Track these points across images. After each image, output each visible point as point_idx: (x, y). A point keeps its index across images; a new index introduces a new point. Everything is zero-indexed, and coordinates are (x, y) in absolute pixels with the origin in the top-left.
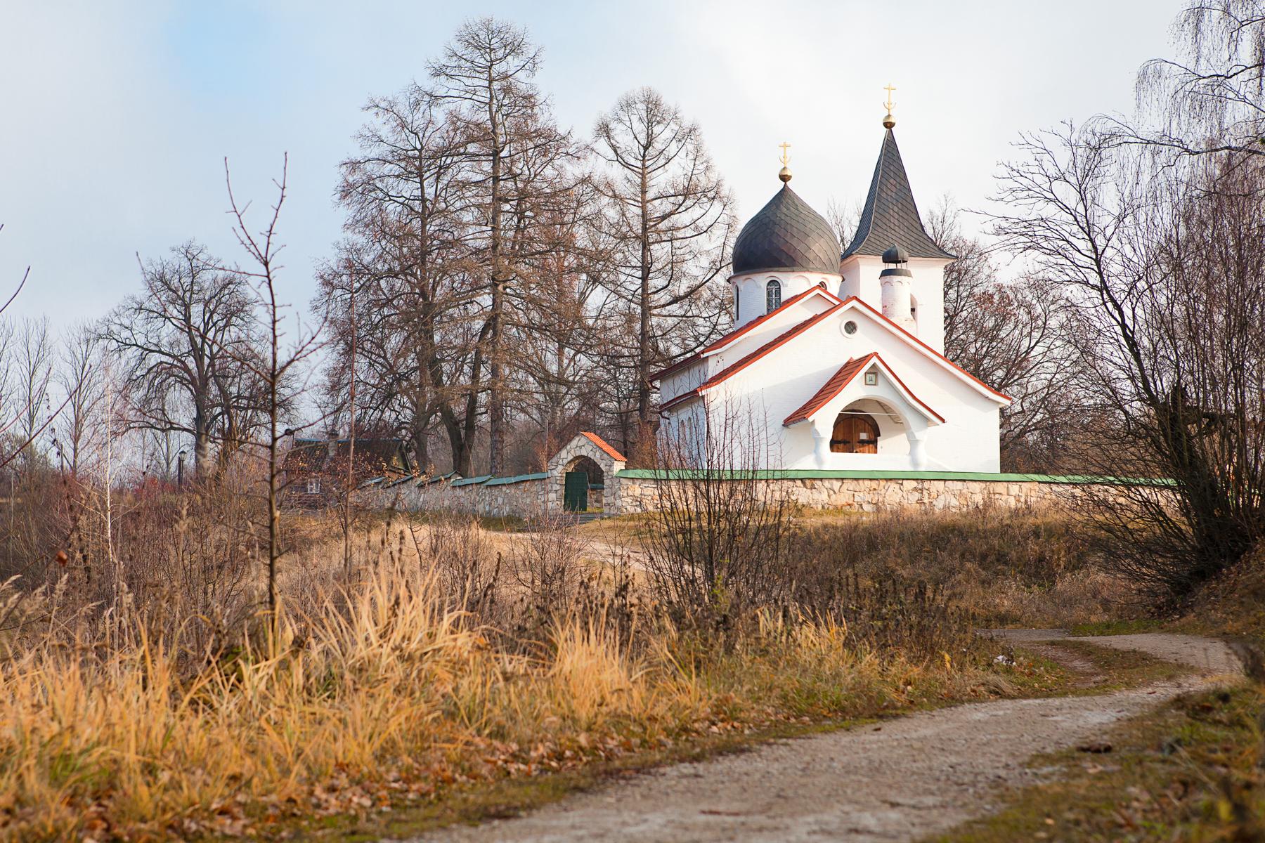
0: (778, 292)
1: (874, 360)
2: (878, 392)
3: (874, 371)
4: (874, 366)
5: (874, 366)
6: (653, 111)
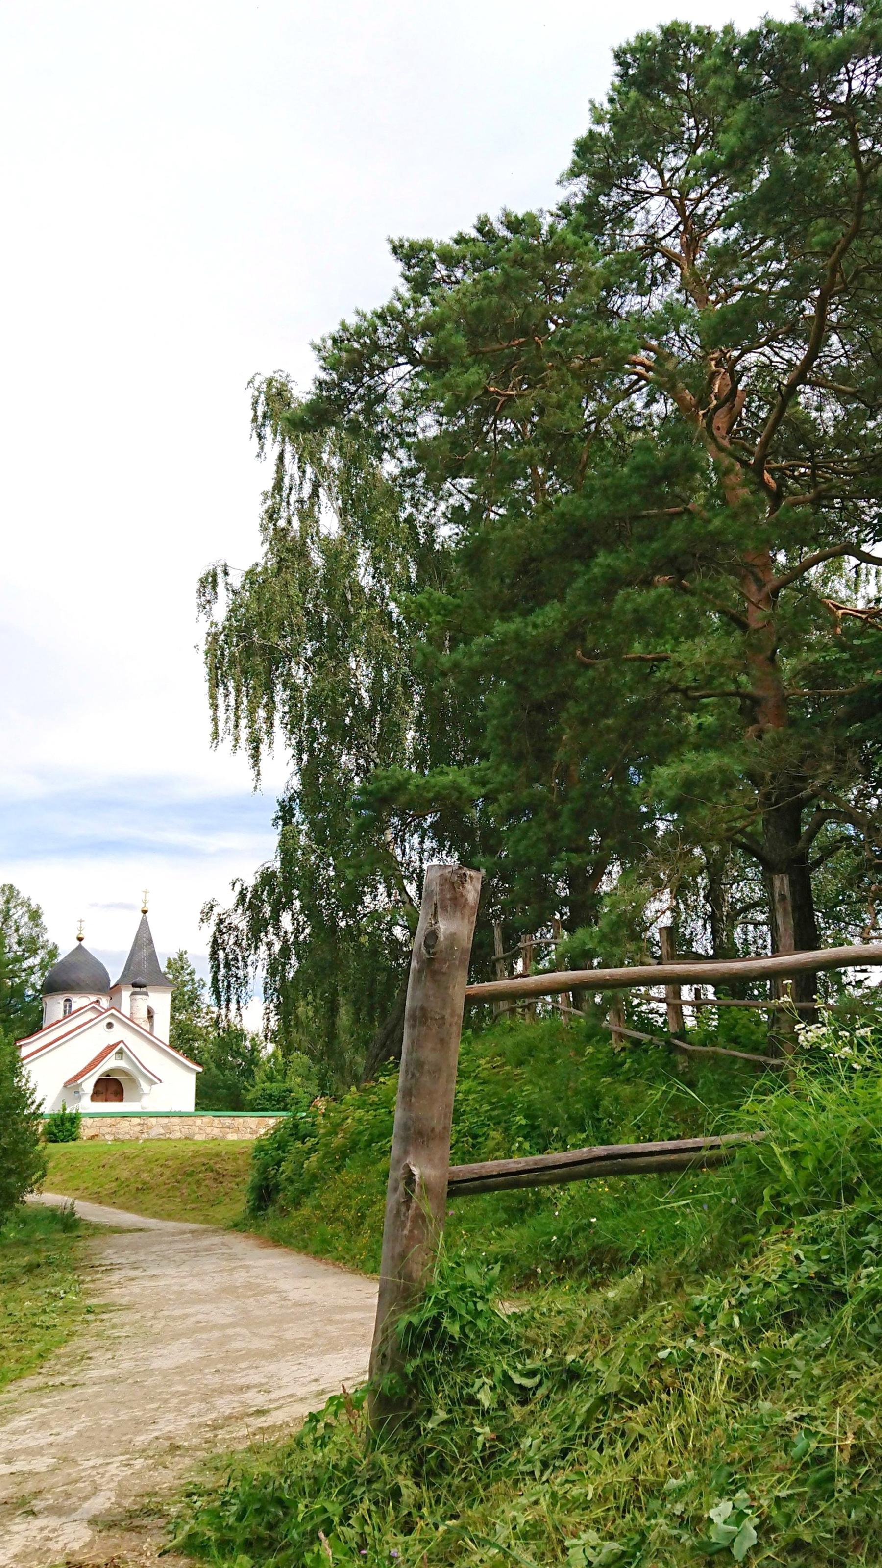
0: (70, 1006)
1: (121, 1045)
2: (122, 1064)
3: (121, 1052)
4: (121, 1049)
5: (121, 1049)
6: (11, 887)
